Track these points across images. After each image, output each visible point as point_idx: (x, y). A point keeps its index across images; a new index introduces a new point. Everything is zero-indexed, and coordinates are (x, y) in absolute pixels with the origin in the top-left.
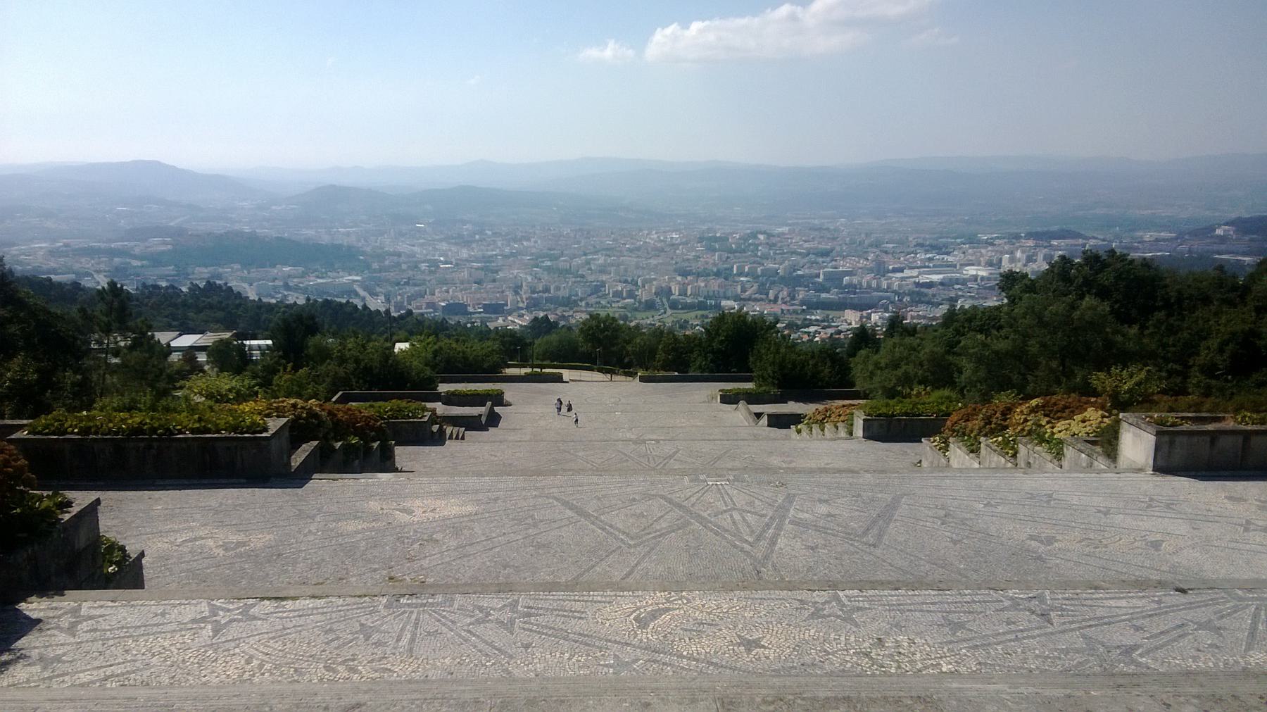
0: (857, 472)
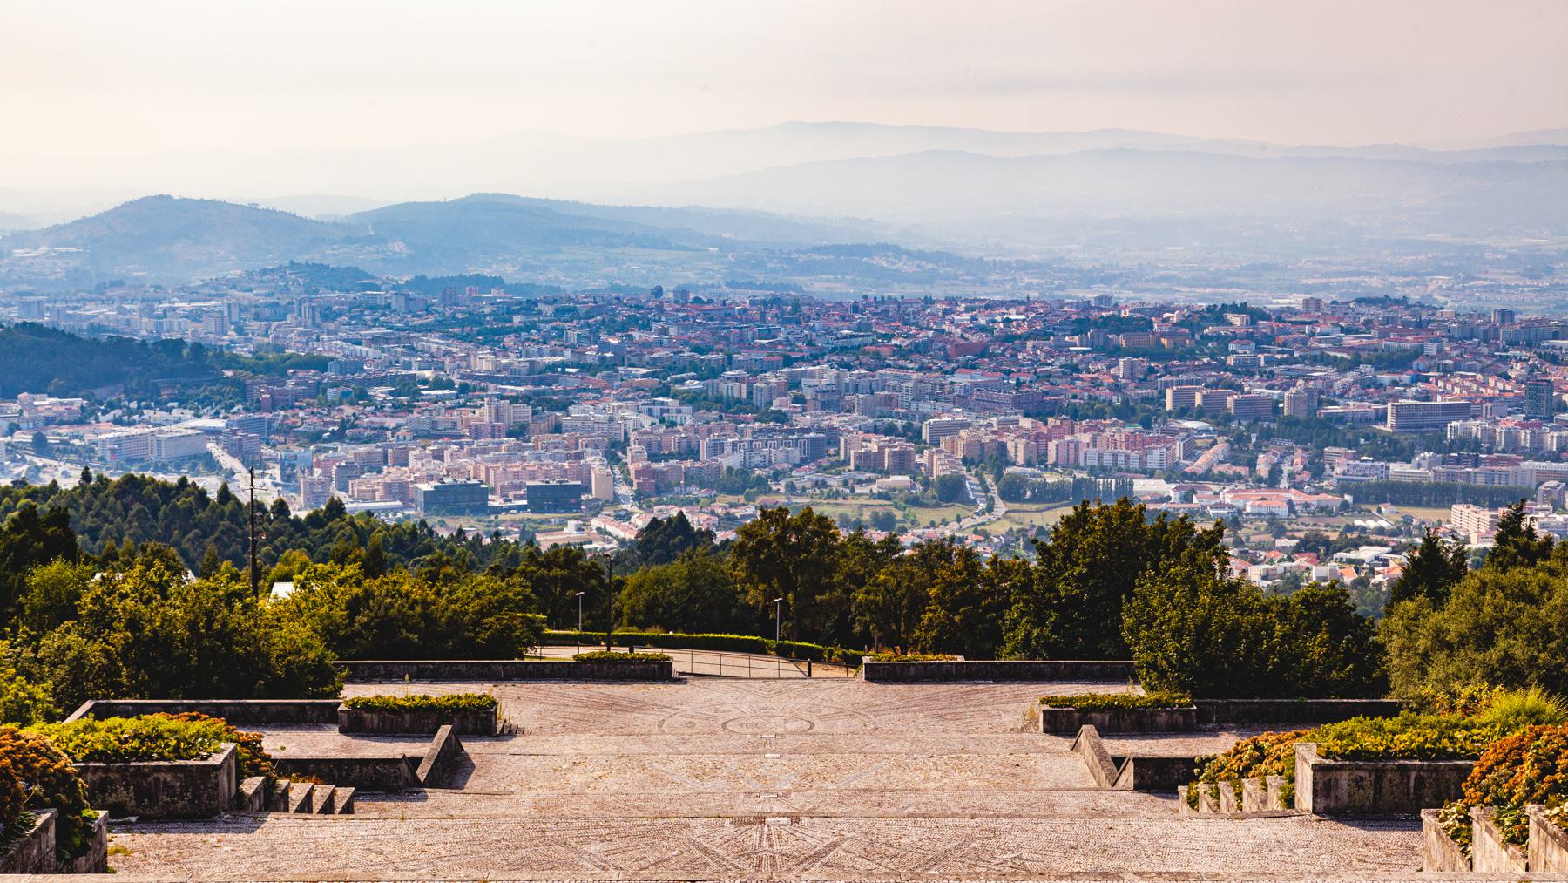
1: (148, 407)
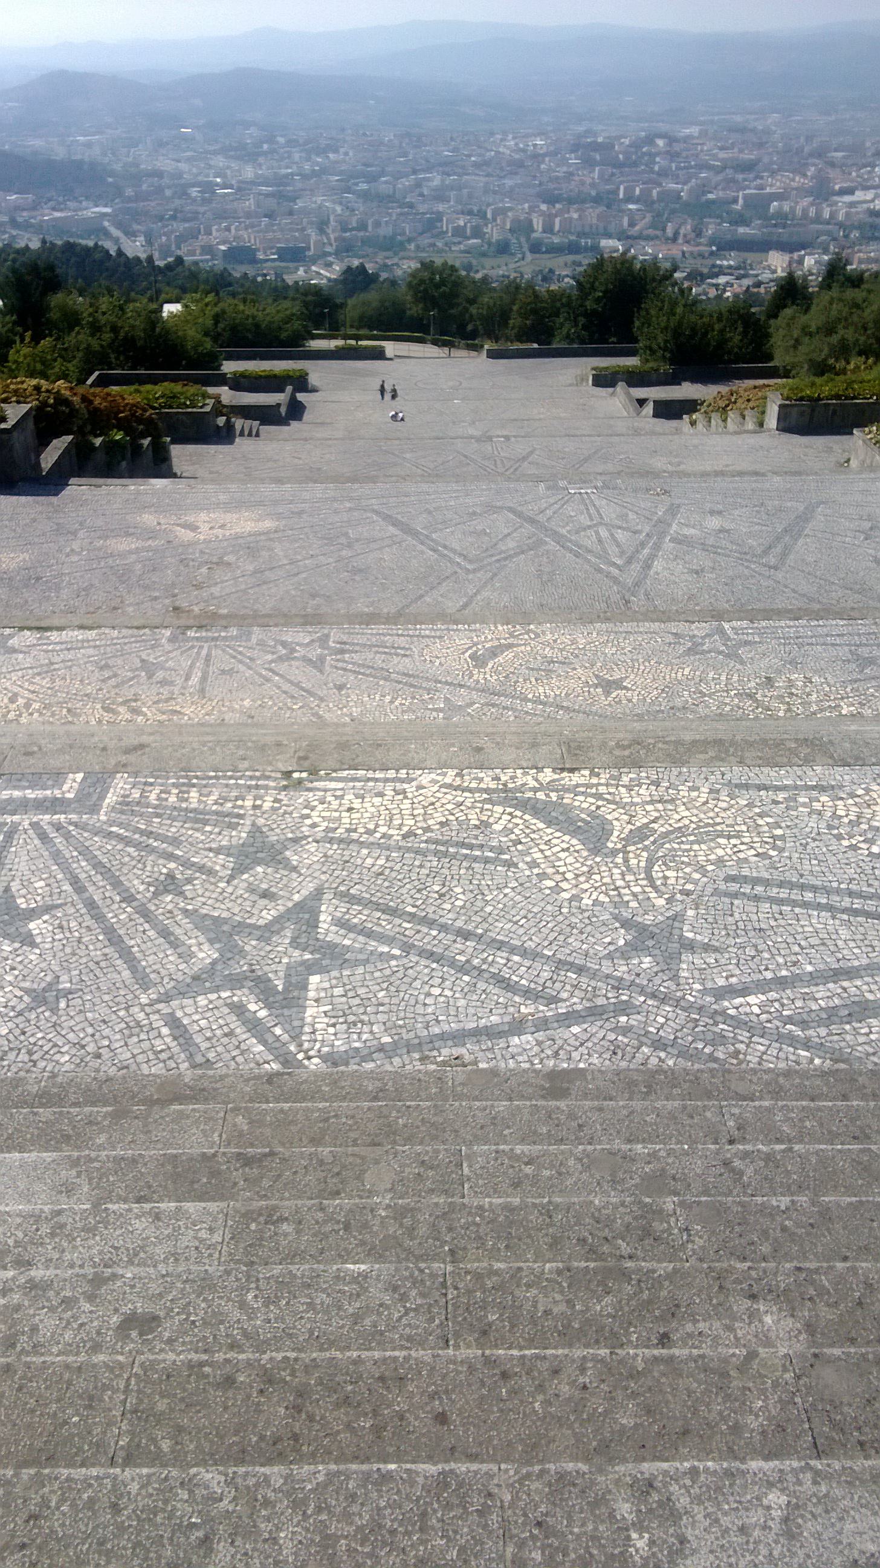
0: (763, 475)
1: (69, 200)
